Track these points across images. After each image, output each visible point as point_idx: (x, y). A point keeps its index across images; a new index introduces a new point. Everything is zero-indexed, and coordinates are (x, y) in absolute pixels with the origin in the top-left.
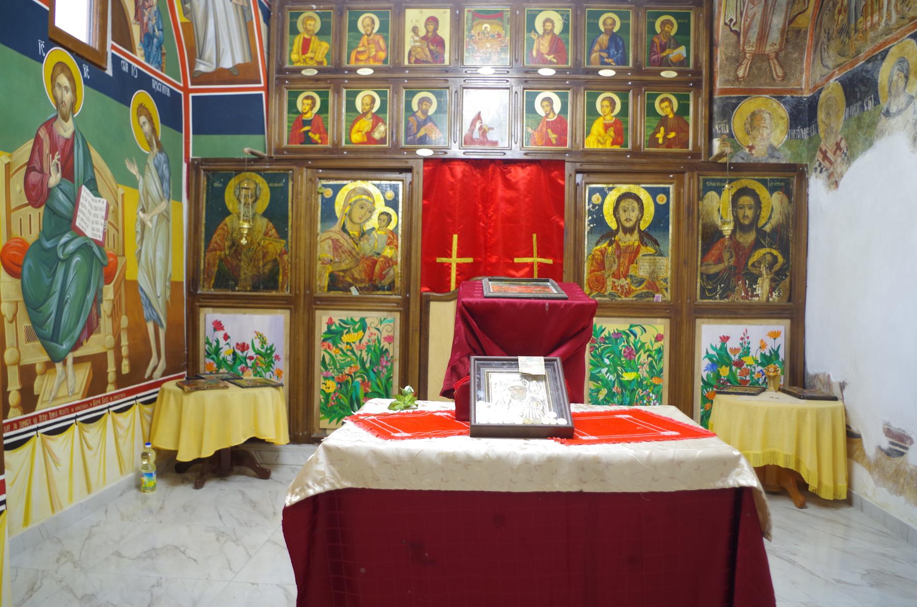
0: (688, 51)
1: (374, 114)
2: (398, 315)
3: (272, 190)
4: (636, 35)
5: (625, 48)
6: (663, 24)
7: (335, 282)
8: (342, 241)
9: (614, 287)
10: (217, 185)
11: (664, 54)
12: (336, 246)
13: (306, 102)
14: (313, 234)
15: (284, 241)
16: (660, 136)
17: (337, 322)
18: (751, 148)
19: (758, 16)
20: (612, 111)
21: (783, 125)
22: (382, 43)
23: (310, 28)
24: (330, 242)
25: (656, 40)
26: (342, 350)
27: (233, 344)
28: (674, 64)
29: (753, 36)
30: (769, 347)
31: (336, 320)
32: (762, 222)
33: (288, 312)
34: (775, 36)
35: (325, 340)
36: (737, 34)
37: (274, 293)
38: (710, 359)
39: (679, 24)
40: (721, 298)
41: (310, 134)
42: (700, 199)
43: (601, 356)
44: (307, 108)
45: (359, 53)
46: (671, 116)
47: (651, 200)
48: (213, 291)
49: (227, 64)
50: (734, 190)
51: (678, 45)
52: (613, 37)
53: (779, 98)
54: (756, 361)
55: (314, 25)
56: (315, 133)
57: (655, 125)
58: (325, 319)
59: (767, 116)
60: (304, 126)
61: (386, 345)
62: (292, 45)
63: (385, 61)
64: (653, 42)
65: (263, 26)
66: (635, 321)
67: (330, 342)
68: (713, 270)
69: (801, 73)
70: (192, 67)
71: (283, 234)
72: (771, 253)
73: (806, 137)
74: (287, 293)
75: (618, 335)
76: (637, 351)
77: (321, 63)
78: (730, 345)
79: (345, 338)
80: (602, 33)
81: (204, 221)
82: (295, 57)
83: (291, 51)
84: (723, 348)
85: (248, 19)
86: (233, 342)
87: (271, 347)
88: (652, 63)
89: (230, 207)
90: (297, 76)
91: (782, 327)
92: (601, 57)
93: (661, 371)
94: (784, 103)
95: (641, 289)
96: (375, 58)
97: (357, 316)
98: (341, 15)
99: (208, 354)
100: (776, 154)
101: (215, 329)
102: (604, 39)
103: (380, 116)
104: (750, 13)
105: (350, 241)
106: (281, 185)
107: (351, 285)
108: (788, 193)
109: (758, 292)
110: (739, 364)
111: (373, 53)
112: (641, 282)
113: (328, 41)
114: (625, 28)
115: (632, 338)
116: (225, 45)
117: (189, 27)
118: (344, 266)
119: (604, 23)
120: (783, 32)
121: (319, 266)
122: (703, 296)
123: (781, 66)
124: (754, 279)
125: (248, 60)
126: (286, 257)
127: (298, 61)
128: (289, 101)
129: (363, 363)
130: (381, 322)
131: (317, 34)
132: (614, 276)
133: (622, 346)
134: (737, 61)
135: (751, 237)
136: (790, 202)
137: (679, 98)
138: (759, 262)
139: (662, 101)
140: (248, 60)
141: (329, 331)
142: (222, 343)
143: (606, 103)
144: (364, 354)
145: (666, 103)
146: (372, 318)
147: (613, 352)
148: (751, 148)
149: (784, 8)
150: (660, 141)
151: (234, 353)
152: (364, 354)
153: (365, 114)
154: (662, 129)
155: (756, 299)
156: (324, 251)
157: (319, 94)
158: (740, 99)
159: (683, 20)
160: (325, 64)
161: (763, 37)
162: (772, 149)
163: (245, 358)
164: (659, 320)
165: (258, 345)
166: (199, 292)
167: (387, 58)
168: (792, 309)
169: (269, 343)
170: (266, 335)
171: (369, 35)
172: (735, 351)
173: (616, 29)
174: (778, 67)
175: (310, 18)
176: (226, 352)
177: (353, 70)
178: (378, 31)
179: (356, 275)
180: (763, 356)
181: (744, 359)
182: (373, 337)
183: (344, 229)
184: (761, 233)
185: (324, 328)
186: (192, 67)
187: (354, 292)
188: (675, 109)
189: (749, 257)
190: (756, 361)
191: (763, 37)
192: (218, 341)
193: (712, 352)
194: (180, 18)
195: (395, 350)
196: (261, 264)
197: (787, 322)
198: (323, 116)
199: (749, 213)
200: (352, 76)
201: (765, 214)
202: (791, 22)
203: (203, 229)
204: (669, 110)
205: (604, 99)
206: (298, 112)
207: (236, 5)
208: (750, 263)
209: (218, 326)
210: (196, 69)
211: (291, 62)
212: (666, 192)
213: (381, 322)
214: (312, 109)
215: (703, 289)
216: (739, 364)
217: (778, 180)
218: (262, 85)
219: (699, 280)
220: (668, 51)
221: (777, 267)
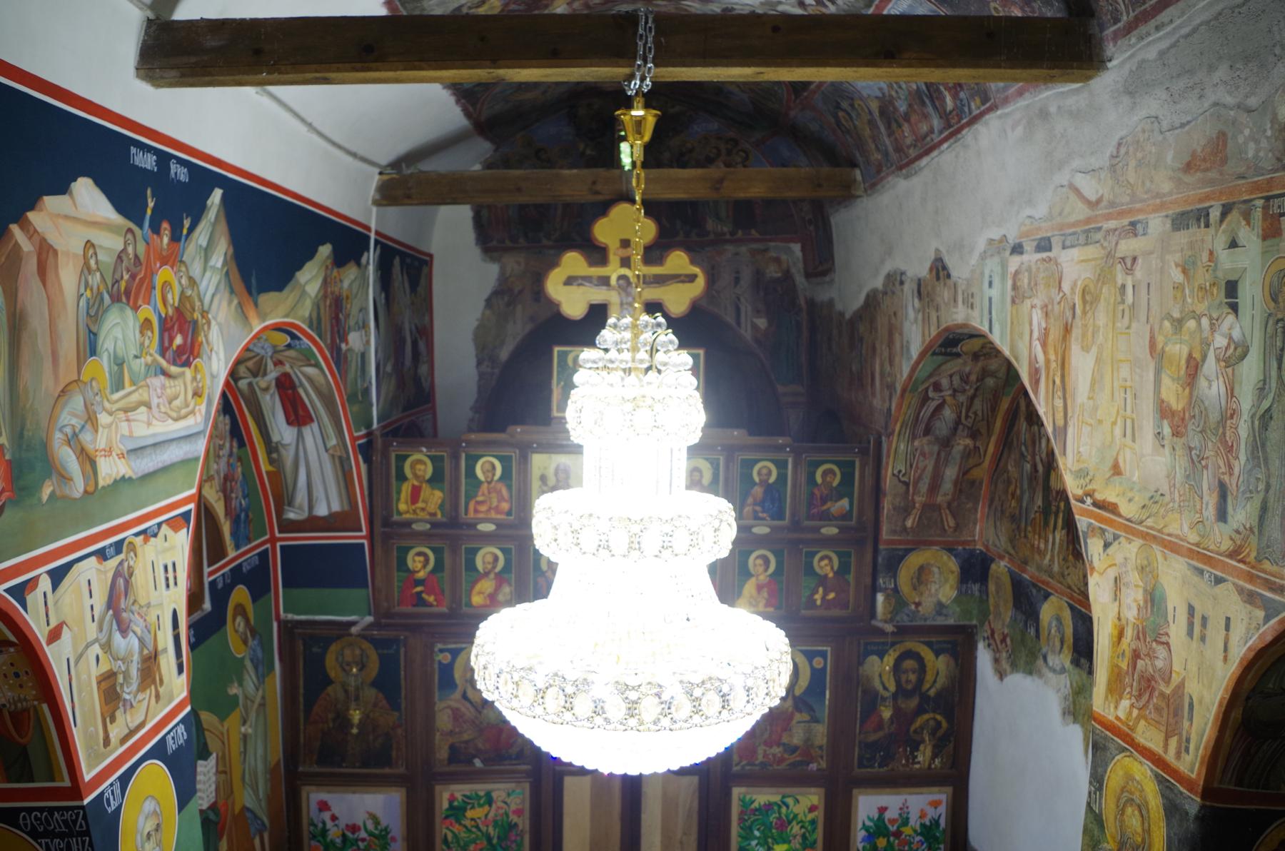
0: (851, 504)
1: (497, 574)
2: (527, 786)
3: (381, 657)
4: (794, 486)
5: (781, 500)
6: (825, 474)
7: (456, 754)
8: (463, 709)
9: (765, 755)
10: (315, 650)
11: (825, 507)
12: (456, 715)
13: (417, 558)
14: (430, 704)
15: (396, 714)
16: (818, 597)
17: (460, 798)
18: (918, 604)
19: (930, 468)
20: (766, 570)
21: (953, 579)
22: (505, 492)
23: (419, 473)
24: (449, 711)
25: (816, 492)
26: (465, 826)
27: (342, 826)
28: (836, 518)
29: (924, 487)
30: (929, 817)
31: (459, 796)
32: (927, 686)
33: (404, 790)
34: (947, 486)
35: (446, 817)
36: (907, 484)
37: (387, 770)
38: (867, 830)
39: (842, 474)
40: (880, 766)
41: (424, 595)
42: (861, 663)
43: (750, 828)
44: (419, 566)
45: (479, 503)
46: (831, 575)
47: (807, 663)
48: (316, 769)
49: (322, 511)
50: (897, 654)
51: (840, 498)
52: (769, 489)
53: (950, 550)
54: (915, 831)
55: (425, 471)
56: (429, 594)
57: (813, 586)
58: (446, 796)
59: (935, 570)
60: (416, 586)
61: (514, 818)
62: (399, 493)
63: (509, 513)
64: (812, 494)
65: (363, 467)
66: (788, 790)
67: (452, 819)
68: (873, 737)
69: (975, 524)
70: (280, 513)
71: (394, 704)
72: (935, 719)
73: (977, 593)
74: (402, 770)
75: (769, 807)
76: (790, 823)
77: (434, 515)
78: (888, 815)
79: (469, 814)
80: (755, 484)
81: (302, 691)
82: (402, 507)
83: (398, 499)
84: (881, 818)
85: (346, 468)
86: (342, 823)
87: (386, 829)
88: (810, 517)
89: (332, 674)
90: (408, 530)
91: (942, 796)
92: (755, 512)
93: (815, 842)
94: (955, 556)
95: (796, 757)
96: (497, 510)
97: (481, 788)
98: (456, 457)
99: (314, 837)
100: (944, 611)
101: (321, 810)
102: (758, 491)
103: (506, 576)
104: (921, 465)
105: (472, 709)
106: (391, 651)
107: (475, 757)
108: (954, 655)
109: (920, 758)
110: (898, 834)
111: (495, 503)
112: (794, 749)
113: (442, 490)
114: (782, 478)
115: (784, 810)
116: (319, 492)
117: (277, 476)
118: (466, 737)
119: (759, 473)
120: (956, 483)
121: (438, 736)
122: (861, 765)
123: (954, 517)
124: (915, 746)
125: (346, 508)
126: (399, 731)
127: (407, 512)
128: (398, 558)
129: (489, 839)
130: (509, 795)
131: (430, 481)
132: (766, 743)
133: (773, 818)
134: (906, 510)
135: (914, 703)
136: (957, 664)
137: (840, 555)
138: (922, 728)
139: (822, 559)
140: (346, 508)
141: (451, 807)
142: (329, 824)
143: (759, 561)
144: (491, 830)
145: (826, 562)
146: (499, 790)
147: (763, 824)
148: (918, 604)
149: (958, 461)
150: (819, 602)
151: (344, 835)
152: (491, 830)
153: (486, 574)
154: (821, 590)
155: (917, 766)
156: (443, 721)
157: (433, 549)
158: (908, 551)
159: (847, 468)
160: (439, 516)
161: (934, 487)
162: (940, 607)
163: (357, 840)
164: (813, 790)
165: (370, 826)
166: (301, 769)
167: (511, 510)
168: (954, 774)
169: (384, 823)
170: (379, 814)
171: (489, 483)
172: (893, 821)
173: (772, 479)
174: (950, 518)
175: (420, 462)
176: (334, 833)
177: (472, 526)
178: (501, 479)
179: (480, 746)
180: (923, 825)
181: (903, 829)
182: (501, 811)
183: (465, 696)
184: (924, 698)
185: (446, 805)
186: (280, 513)
187: (478, 763)
188: (836, 567)
189: (911, 724)
190: (915, 831)
191: (934, 487)
192: (324, 823)
193: (868, 823)
194: (265, 467)
195: (524, 823)
196: (371, 738)
197: (950, 790)
198: (440, 575)
199: (913, 677)
200: (472, 532)
201: (929, 677)
202: (964, 474)
203: (301, 699)
204: (828, 568)
205: (757, 557)
206: (408, 570)
207: (333, 456)
208: (912, 729)
209: (324, 806)
210: (285, 516)
211: (399, 513)
212: (823, 655)
213: (509, 795)
214: (424, 566)
215: (861, 759)
216: (898, 834)
217: (945, 642)
218: (364, 533)
219: (857, 749)
220: (829, 504)
221: (940, 733)
